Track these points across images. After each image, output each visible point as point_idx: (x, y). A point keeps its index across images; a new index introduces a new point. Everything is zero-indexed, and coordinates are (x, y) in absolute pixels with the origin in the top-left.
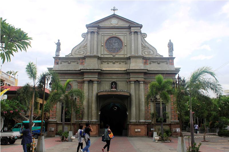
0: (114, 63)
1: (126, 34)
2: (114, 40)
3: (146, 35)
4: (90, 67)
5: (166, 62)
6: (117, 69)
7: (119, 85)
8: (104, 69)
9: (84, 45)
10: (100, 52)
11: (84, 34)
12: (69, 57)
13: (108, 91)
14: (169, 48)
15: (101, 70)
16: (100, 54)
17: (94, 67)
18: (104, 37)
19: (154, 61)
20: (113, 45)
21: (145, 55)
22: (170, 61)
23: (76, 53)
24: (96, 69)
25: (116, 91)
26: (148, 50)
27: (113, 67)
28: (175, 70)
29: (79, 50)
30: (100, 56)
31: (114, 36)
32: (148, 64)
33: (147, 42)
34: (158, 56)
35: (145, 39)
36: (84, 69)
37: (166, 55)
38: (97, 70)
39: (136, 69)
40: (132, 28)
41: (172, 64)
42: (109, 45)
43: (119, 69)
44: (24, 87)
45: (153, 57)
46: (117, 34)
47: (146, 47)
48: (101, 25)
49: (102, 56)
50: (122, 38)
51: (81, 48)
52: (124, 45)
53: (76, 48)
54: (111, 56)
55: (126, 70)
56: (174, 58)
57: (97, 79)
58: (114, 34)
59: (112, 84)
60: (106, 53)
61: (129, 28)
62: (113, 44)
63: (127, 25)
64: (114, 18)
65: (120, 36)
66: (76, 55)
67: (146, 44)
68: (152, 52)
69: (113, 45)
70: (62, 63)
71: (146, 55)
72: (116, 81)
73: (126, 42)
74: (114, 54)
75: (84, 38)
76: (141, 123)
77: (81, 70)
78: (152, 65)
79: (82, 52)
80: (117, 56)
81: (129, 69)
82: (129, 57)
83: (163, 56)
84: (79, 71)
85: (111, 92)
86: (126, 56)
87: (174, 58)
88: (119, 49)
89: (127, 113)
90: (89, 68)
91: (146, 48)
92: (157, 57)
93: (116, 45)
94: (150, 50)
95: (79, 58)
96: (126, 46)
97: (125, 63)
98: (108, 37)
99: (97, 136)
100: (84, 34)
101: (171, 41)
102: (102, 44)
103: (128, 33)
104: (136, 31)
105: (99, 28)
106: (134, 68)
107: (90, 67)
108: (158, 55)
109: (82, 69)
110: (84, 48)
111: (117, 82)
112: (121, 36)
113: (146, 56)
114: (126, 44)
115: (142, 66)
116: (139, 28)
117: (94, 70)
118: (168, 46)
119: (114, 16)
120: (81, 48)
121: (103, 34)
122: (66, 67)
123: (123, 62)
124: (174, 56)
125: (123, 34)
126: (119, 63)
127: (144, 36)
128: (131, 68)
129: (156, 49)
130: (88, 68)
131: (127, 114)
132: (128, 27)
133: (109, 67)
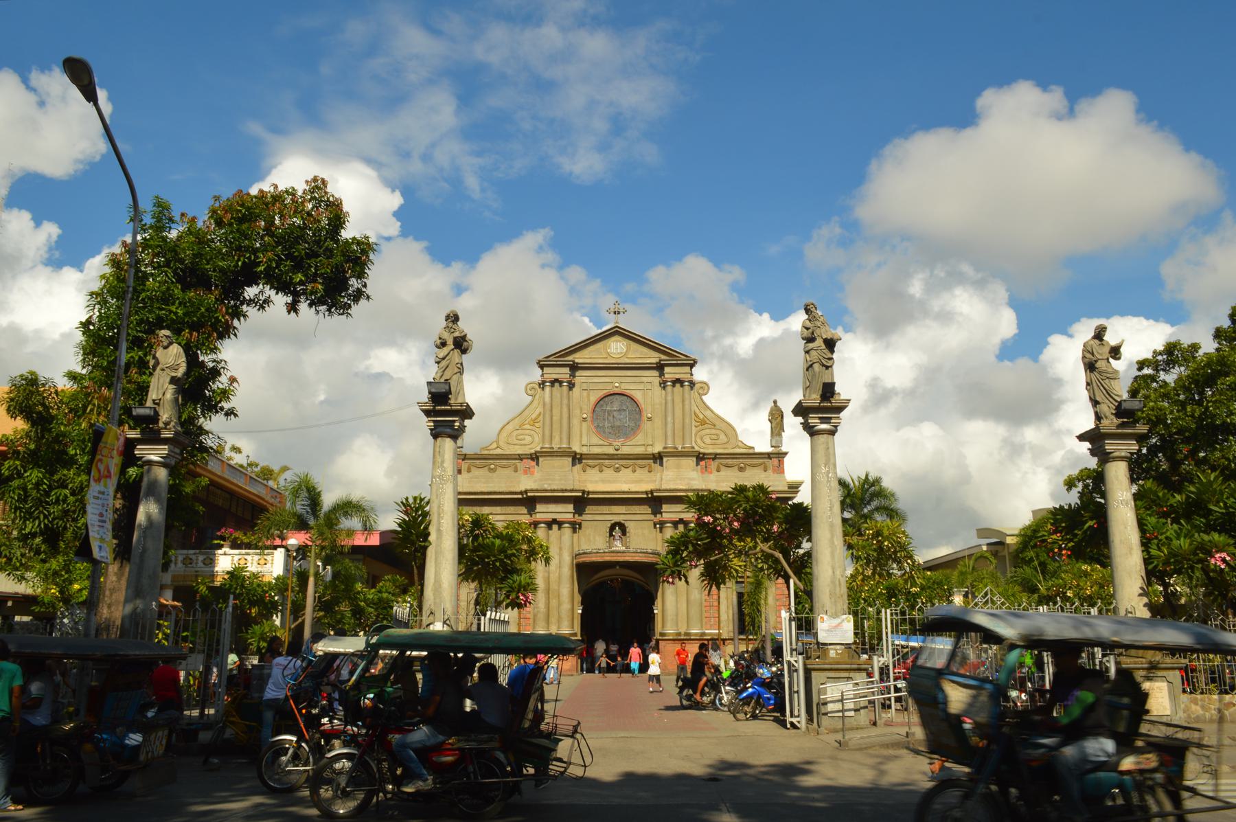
18: (589, 395)
22: (775, 461)
41: (780, 469)
47: (708, 421)
49: (585, 450)
50: (638, 396)
54: (611, 451)
56: (786, 454)
57: (571, 516)
80: (625, 450)
87: (786, 454)
96: (650, 419)
98: (601, 394)
102: (585, 416)
131: (655, 611)
132: (657, 363)
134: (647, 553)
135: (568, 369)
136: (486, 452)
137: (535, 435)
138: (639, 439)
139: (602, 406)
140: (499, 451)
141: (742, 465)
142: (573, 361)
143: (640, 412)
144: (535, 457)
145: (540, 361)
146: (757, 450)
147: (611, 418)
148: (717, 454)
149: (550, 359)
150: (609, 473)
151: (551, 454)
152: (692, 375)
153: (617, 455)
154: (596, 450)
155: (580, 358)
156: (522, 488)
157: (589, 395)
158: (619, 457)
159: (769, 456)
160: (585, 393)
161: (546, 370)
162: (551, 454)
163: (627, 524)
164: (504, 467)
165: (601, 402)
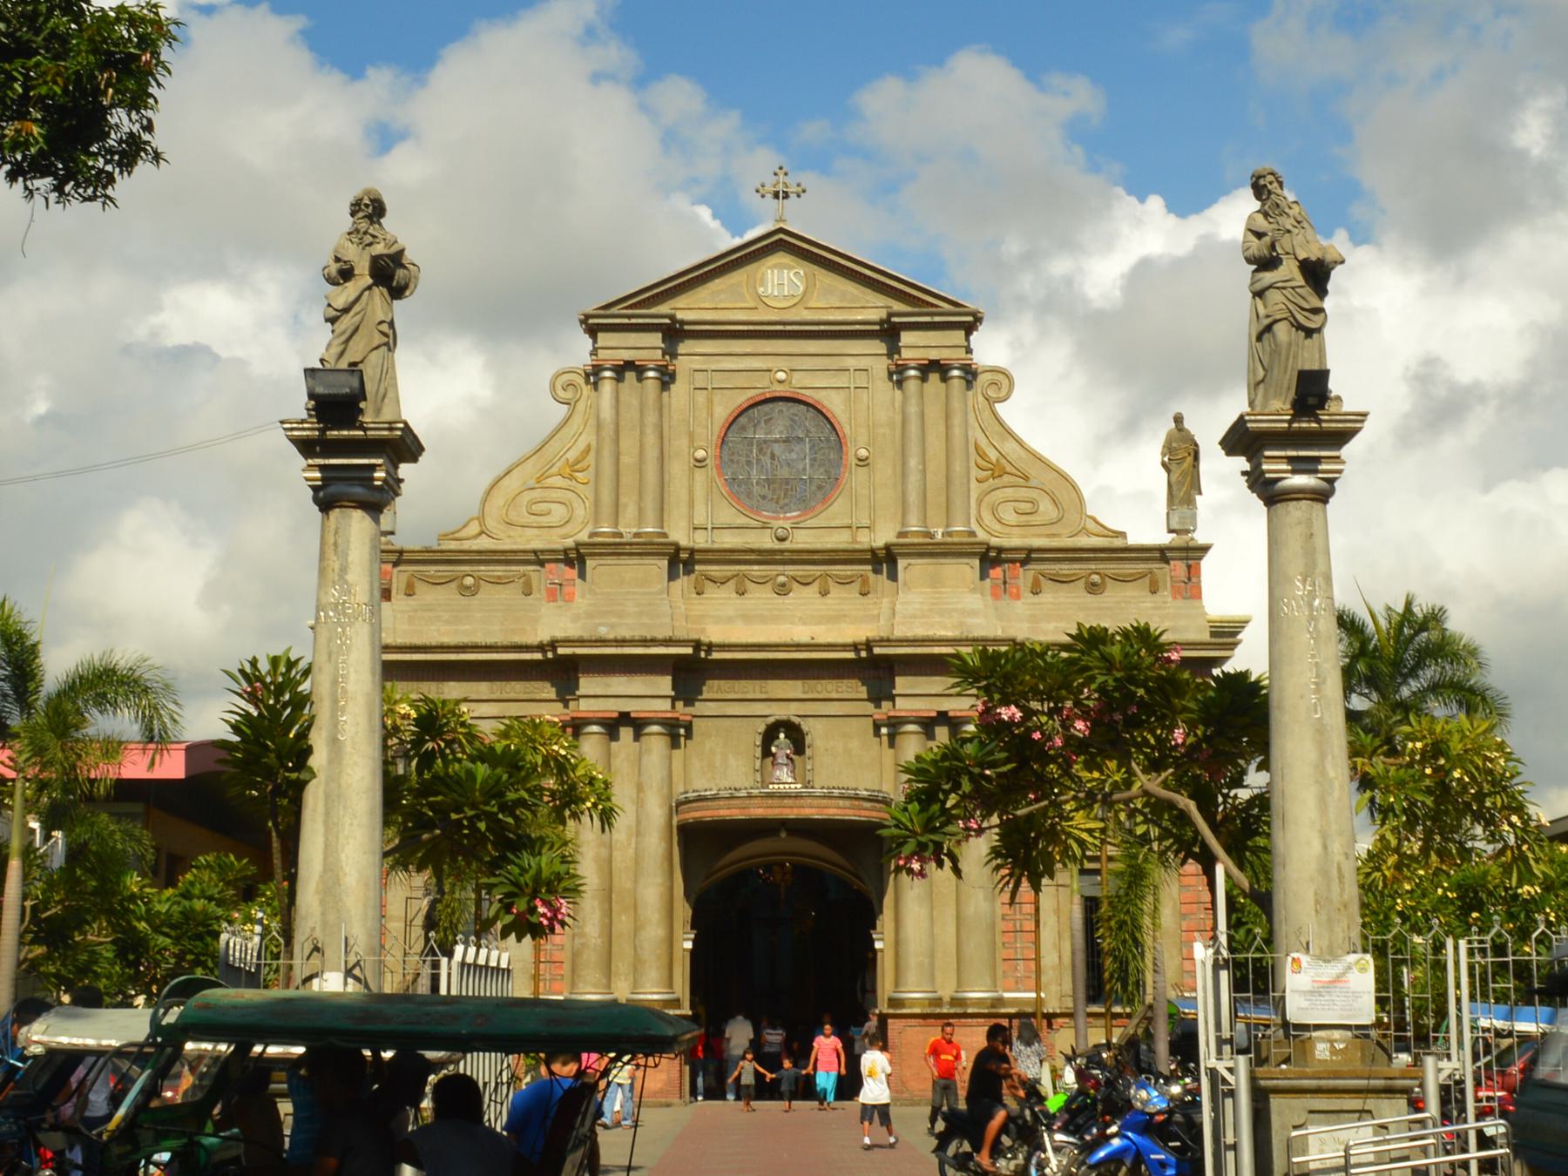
0: (782, 590)
1: (861, 380)
2: (780, 423)
3: (1005, 382)
4: (614, 620)
5: (1147, 580)
6: (802, 634)
7: (819, 743)
8: (714, 634)
9: (572, 455)
10: (684, 510)
11: (565, 377)
12: (466, 545)
13: (750, 797)
14: (1168, 471)
15: (697, 645)
16: (683, 524)
17: (645, 620)
18: (710, 402)
19: (1065, 569)
20: (773, 457)
21: (998, 527)
22: (1179, 568)
23: (513, 517)
24: (660, 636)
25: (798, 796)
26: (1023, 493)
27: (776, 619)
28: (1206, 637)
29: (536, 494)
30: (684, 542)
31: (780, 390)
32: (1018, 597)
33: (1010, 433)
34: (1089, 534)
35: (997, 406)
36: (581, 642)
37: (1148, 529)
38: (668, 642)
39: (734, 639)
40: (907, 338)
41: (1190, 587)
42: (743, 459)
43: (825, 635)
44: (312, 48)
45: (1055, 543)
46: (799, 380)
47: (1009, 468)
48: (688, 308)
49: (701, 541)
50: (834, 404)
51: (549, 481)
52: (854, 461)
53: (512, 483)
54: (766, 541)
55: (868, 645)
56: (1205, 549)
57: (665, 705)
58: (781, 375)
59: (769, 736)
60: (727, 514)
61: (889, 332)
62: (778, 449)
63: (873, 308)
64: (781, 258)
65: (824, 393)
66: (514, 532)
67: (1009, 447)
68: (1046, 508)
69: (773, 457)
70: (420, 587)
71: (1008, 530)
72: (796, 720)
73: (862, 440)
74: (781, 523)
75: (563, 410)
76: (970, 1011)
77: (553, 645)
78: (1042, 598)
79: (559, 512)
80: (802, 540)
81: (888, 640)
82: (888, 548)
83: (1123, 535)
84: (541, 647)
85: (770, 802)
86: (865, 540)
87: (1205, 549)
88: (827, 487)
89: (872, 942)
90: (612, 626)
91: (1006, 478)
92: (1084, 541)
93: (800, 461)
94: (1034, 494)
95: (535, 552)
96: (863, 462)
97: (856, 586)
98: (742, 398)
99: (670, 1100)
100: (565, 377)
101: (1187, 425)
102: (700, 454)
103: (881, 366)
104: (934, 355)
105: (674, 333)
106: (920, 631)
107: (614, 620)
108: (1091, 525)
109: (568, 642)
110: (571, 478)
111: (805, 728)
112: (833, 393)
113: (1009, 536)
114: (863, 453)
115: (973, 613)
116: (958, 336)
117: (645, 642)
118: (1164, 465)
119: (781, 230)
120: (549, 481)
121: (700, 380)
122: (446, 616)
123: (844, 582)
124: (1200, 538)
125: (841, 381)
126: (815, 586)
127: (992, 393)
128: (899, 633)
129: (1074, 487)
130: (603, 632)
131: (878, 945)
132: (881, 322)
133: (747, 618)
134: (857, 798)
135: (660, 335)
136: (453, 545)
137: (577, 504)
138: (838, 511)
139: (743, 428)
140: (484, 543)
141: (1096, 578)
142: (672, 317)
143: (840, 444)
144: (575, 558)
145: (587, 317)
146: (1133, 540)
147: (766, 460)
148: (1030, 550)
149: (614, 310)
150: (761, 597)
151: (616, 549)
152: (969, 351)
153: (782, 552)
154: (728, 540)
155: (689, 308)
156: (544, 636)
157: (710, 402)
158: (787, 556)
159: (1162, 554)
160: (701, 397)
161: (604, 339)
162: (616, 549)
163: (806, 726)
164: (498, 582)
165: (743, 420)
